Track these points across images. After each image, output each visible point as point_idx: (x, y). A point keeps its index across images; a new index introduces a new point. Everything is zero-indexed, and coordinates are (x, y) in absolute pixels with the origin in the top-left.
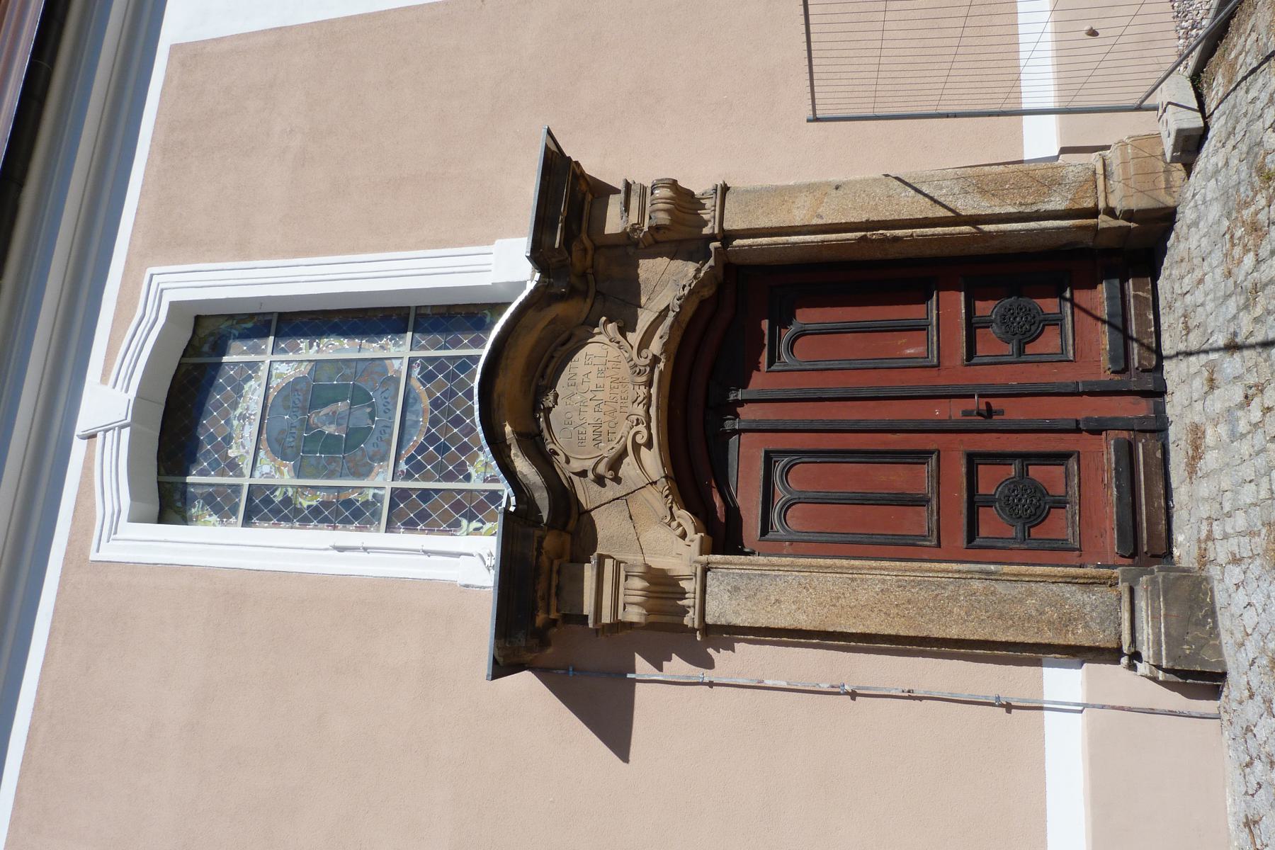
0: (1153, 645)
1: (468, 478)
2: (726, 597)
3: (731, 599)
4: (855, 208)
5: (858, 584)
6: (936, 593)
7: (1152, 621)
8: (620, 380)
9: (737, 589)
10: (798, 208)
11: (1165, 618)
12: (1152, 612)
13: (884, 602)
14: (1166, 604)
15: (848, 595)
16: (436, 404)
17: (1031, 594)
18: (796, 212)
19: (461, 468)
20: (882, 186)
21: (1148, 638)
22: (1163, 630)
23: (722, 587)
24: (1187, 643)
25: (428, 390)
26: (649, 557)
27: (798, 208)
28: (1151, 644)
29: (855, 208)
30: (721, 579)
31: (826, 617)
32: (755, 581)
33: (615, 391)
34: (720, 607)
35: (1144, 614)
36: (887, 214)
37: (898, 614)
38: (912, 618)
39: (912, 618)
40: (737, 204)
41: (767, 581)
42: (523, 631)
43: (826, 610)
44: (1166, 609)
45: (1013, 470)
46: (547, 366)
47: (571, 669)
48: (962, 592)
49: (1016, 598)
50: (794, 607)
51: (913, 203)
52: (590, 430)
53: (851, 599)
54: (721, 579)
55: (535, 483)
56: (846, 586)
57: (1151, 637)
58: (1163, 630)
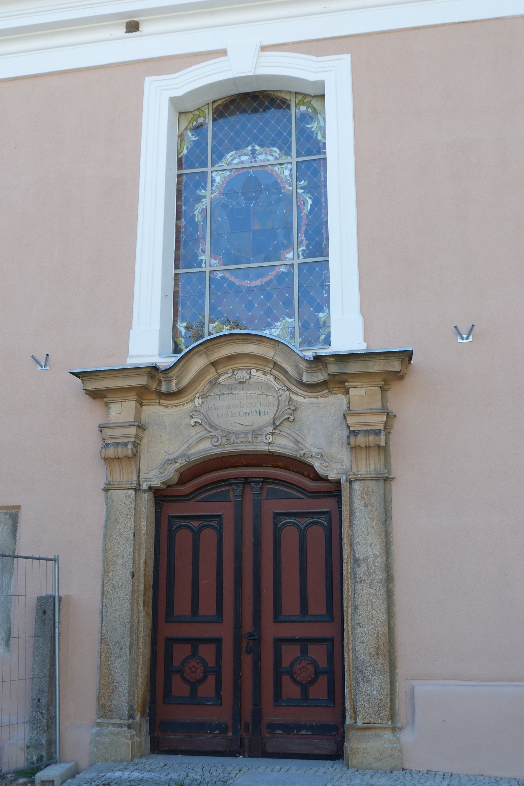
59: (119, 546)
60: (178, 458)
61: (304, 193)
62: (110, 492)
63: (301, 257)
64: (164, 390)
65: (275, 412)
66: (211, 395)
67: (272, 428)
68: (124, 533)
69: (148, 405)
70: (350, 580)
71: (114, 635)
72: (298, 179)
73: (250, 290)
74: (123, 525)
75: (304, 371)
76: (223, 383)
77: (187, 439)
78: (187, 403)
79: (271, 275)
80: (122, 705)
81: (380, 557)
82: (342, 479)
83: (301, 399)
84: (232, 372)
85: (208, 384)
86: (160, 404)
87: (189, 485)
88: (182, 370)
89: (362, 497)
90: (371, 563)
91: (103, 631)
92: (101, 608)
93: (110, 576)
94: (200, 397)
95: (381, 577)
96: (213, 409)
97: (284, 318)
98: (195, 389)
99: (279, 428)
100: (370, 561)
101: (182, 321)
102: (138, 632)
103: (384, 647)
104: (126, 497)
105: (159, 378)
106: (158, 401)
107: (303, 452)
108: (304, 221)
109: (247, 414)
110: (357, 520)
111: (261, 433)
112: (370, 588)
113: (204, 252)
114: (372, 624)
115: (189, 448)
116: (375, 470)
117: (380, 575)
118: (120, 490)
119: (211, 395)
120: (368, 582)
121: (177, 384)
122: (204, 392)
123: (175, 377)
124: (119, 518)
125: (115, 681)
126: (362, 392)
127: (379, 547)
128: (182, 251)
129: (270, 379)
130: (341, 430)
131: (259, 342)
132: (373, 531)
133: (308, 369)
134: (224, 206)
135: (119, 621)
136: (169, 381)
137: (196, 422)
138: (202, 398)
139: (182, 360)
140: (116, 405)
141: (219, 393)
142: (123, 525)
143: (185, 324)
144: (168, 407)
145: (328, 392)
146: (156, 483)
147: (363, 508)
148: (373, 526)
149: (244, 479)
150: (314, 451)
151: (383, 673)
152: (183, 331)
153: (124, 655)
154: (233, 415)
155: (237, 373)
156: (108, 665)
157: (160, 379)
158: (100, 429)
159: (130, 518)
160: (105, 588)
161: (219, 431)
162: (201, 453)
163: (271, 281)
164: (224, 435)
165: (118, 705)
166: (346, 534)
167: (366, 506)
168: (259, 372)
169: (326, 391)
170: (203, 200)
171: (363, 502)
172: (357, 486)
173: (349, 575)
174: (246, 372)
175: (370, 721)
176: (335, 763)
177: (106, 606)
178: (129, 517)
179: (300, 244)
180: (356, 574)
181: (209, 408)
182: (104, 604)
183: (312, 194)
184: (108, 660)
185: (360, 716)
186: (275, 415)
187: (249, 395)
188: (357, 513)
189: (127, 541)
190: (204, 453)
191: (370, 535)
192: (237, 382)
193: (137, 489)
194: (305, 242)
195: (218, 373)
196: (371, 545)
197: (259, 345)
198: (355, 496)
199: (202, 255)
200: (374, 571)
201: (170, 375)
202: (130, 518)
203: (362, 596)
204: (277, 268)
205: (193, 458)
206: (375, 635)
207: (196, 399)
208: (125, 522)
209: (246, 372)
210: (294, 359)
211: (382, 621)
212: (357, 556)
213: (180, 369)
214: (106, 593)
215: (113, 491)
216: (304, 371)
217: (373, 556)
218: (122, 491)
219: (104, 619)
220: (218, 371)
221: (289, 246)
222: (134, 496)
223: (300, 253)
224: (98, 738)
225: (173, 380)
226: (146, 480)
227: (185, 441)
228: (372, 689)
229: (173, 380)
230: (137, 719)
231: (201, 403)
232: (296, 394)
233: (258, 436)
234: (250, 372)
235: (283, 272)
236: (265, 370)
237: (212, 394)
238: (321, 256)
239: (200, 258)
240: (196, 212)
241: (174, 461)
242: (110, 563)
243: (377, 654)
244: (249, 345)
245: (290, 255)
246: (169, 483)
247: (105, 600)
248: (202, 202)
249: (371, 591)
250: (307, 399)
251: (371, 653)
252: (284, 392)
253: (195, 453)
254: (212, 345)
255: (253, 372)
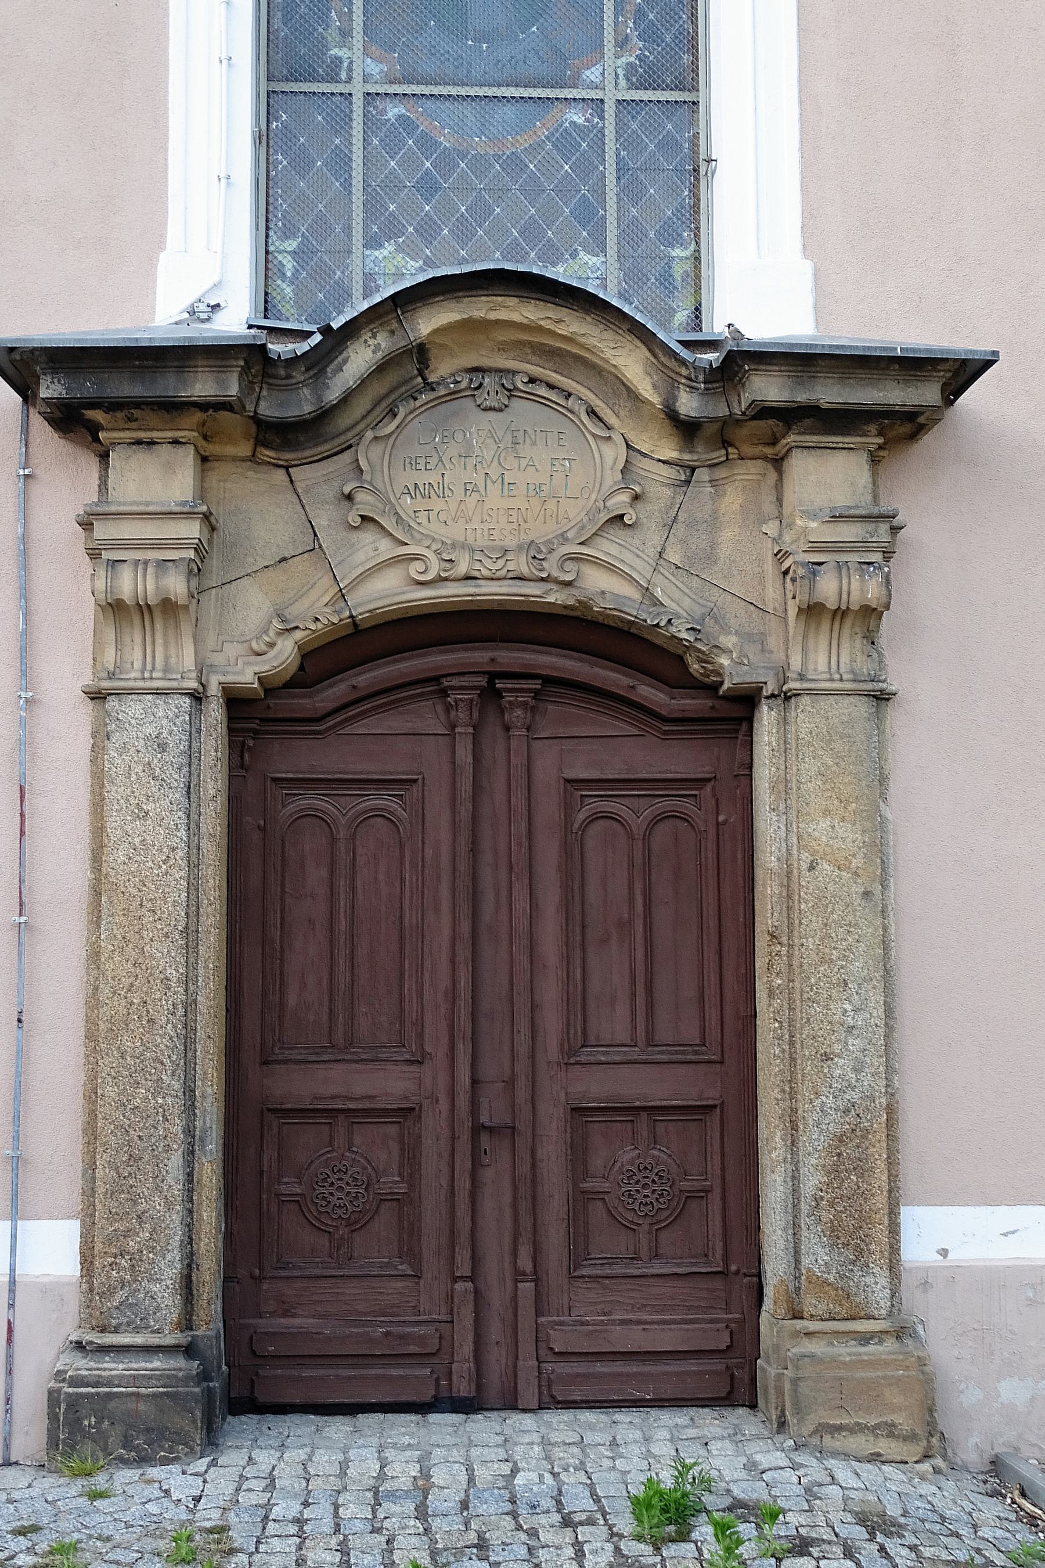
0: (95, 1376)
1: (372, 242)
2: (149, 730)
3: (147, 738)
4: (826, 925)
5: (177, 940)
6: (167, 1062)
7: (131, 1376)
8: (524, 526)
9: (163, 747)
10: (833, 827)
11: (132, 1394)
12: (144, 1376)
13: (149, 982)
14: (154, 1395)
15: (159, 927)
16: (514, 164)
17: (169, 1205)
18: (824, 824)
19: (392, 230)
20: (866, 971)
21: (105, 1370)
22: (116, 1390)
23: (165, 722)
24: (99, 1422)
25: (541, 145)
26: (217, 594)
27: (833, 827)
28: (97, 1372)
29: (826, 925)
30: (178, 722)
31: (123, 893)
32: (176, 776)
33: (503, 520)
34: (133, 722)
35: (143, 1365)
36: (813, 980)
37: (132, 1004)
38: (127, 1025)
39: (127, 1025)
40: (846, 719)
41: (177, 795)
42: (64, 392)
43: (135, 891)
44: (148, 1395)
45: (392, 1182)
46: (551, 387)
47: (27, 472)
48: (169, 1100)
49: (163, 1181)
50: (137, 841)
51: (830, 1023)
52: (433, 478)
53: (152, 932)
54: (178, 722)
55: (328, 387)
56: (173, 923)
57: (106, 1373)
58: (116, 1390)
62: (112, 703)
63: (623, 82)
87: (444, 657)
97: (574, 255)
113: (345, 34)
116: (852, 672)
152: (289, 265)
176: (822, 1437)
179: (622, 43)
193: (198, 697)
204: (556, 110)
223: (620, 71)
235: (573, 123)
238: (680, 87)
239: (335, 52)
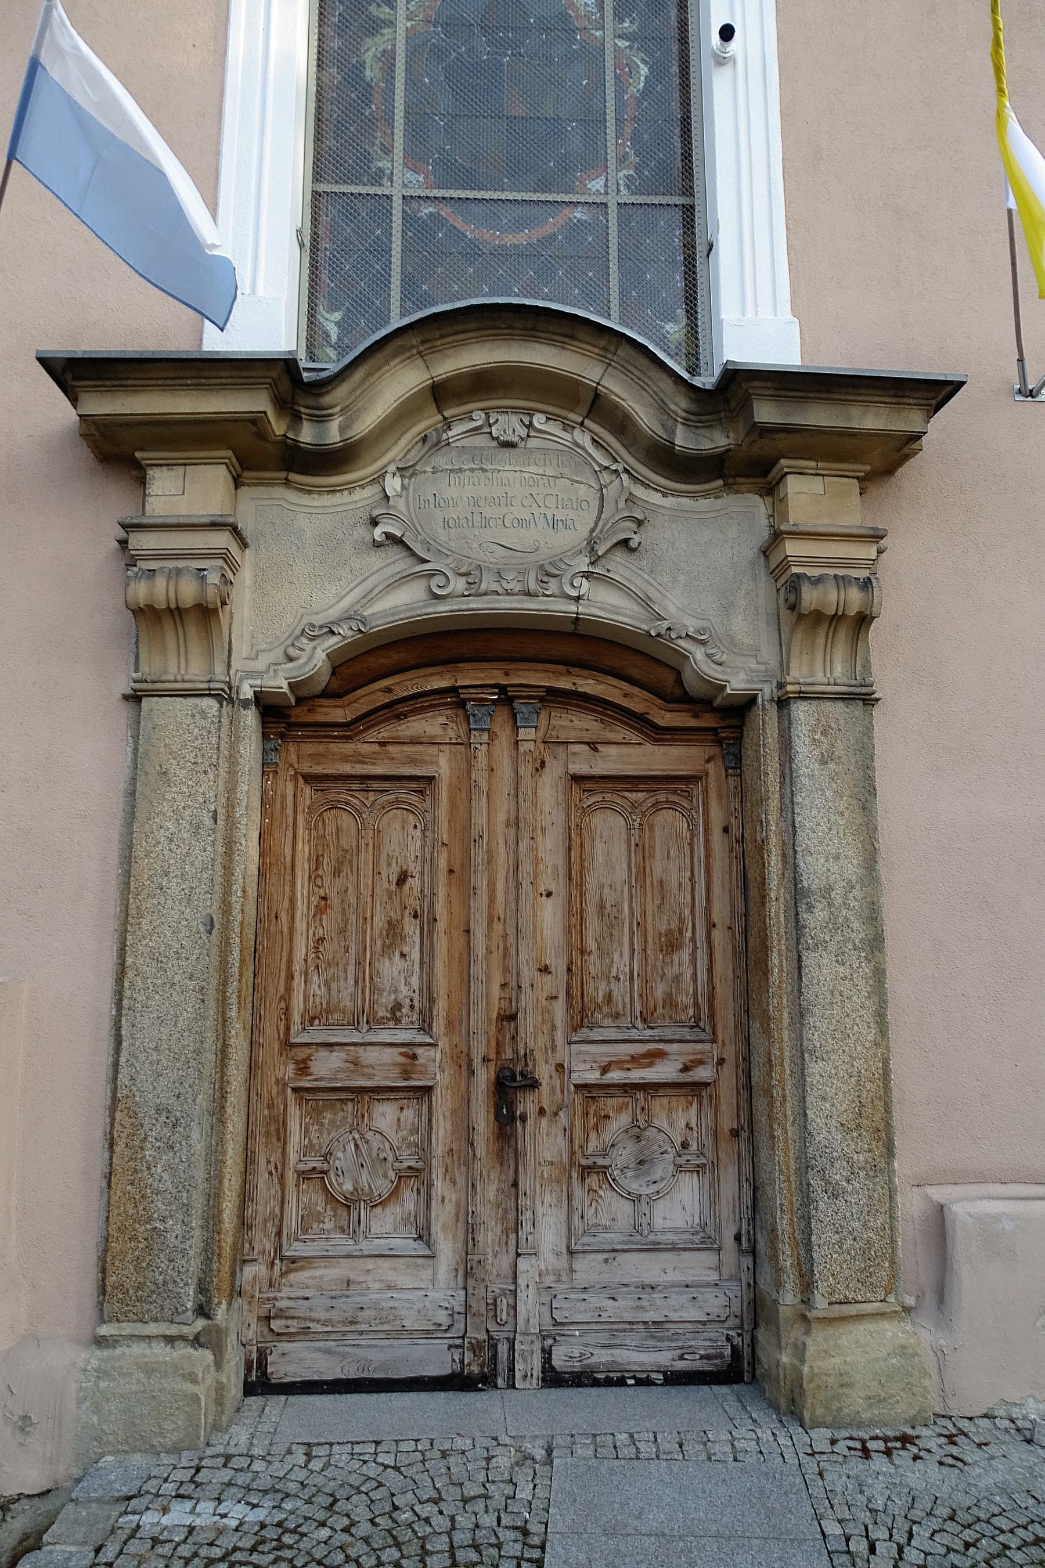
59: (173, 847)
60: (338, 622)
61: (630, 47)
64: (308, 440)
65: (592, 525)
66: (425, 472)
67: (587, 560)
68: (188, 812)
69: (255, 485)
70: (783, 942)
71: (155, 1088)
72: (618, 17)
73: (501, 254)
74: (185, 789)
75: (679, 420)
76: (459, 444)
77: (361, 578)
78: (362, 487)
79: (553, 224)
80: (175, 1281)
81: (858, 887)
82: (760, 696)
83: (655, 498)
84: (483, 415)
85: (417, 443)
86: (287, 483)
88: (358, 393)
89: (814, 740)
90: (839, 901)
91: (120, 1076)
92: (114, 1012)
93: (144, 927)
94: (398, 474)
95: (862, 935)
96: (432, 505)
98: (384, 454)
99: (603, 561)
100: (837, 896)
101: (332, 309)
102: (222, 1077)
103: (874, 1107)
104: (193, 716)
105: (297, 408)
106: (283, 474)
107: (666, 624)
108: (630, 112)
109: (520, 522)
110: (803, 795)
111: (558, 572)
112: (837, 961)
114: (844, 1051)
115: (368, 598)
117: (859, 932)
118: (177, 699)
119: (425, 472)
120: (833, 947)
121: (342, 429)
122: (409, 461)
123: (338, 409)
124: (173, 771)
125: (155, 1215)
126: (814, 486)
127: (855, 862)
128: (330, 142)
129: (581, 442)
130: (755, 578)
131: (566, 340)
132: (841, 822)
133: (691, 417)
134: (438, 53)
135: (169, 1049)
136: (321, 419)
137: (388, 536)
138: (401, 476)
139: (357, 367)
140: (171, 473)
141: (449, 467)
142: (185, 789)
143: (337, 316)
144: (310, 492)
145: (725, 485)
146: (279, 682)
147: (817, 766)
148: (840, 810)
149: (496, 690)
150: (691, 625)
151: (872, 1173)
152: (334, 332)
153: (184, 1143)
154: (486, 523)
155: (497, 420)
156: (136, 1171)
157: (300, 412)
158: (121, 534)
159: (205, 772)
160: (129, 960)
161: (449, 560)
162: (401, 612)
163: (552, 237)
164: (462, 570)
165: (165, 1282)
166: (773, 828)
167: (823, 762)
168: (551, 422)
169: (720, 482)
170: (385, 31)
171: (817, 752)
172: (801, 711)
173: (783, 930)
174: (521, 420)
175: (846, 1297)
177: (130, 1009)
178: (201, 768)
179: (622, 159)
180: (804, 927)
181: (422, 502)
182: (125, 1002)
183: (651, 55)
184: (136, 1159)
185: (822, 1287)
186: (592, 530)
187: (527, 475)
188: (802, 778)
189: (196, 833)
190: (409, 614)
191: (834, 832)
192: (494, 444)
194: (633, 158)
195: (445, 419)
196: (837, 858)
197: (563, 348)
198: (799, 737)
199: (381, 159)
200: (847, 919)
201: (327, 400)
202: (205, 772)
203: (819, 982)
204: (567, 211)
205: (380, 624)
206: (852, 1080)
207: (388, 477)
208: (190, 783)
209: (521, 420)
210: (655, 389)
211: (867, 1045)
212: (805, 884)
213: (353, 390)
214: (130, 974)
215: (157, 699)
216: (679, 420)
217: (843, 884)
218: (182, 699)
219: (125, 1044)
220: (447, 414)
221: (596, 163)
222: (216, 714)
224: (103, 1384)
225: (332, 415)
226: (249, 674)
227: (356, 582)
228: (847, 1215)
229: (332, 415)
230: (219, 1317)
231: (399, 489)
232: (642, 483)
233: (551, 579)
234: (531, 422)
236: (565, 421)
237: (429, 469)
240: (368, 57)
241: (326, 630)
242: (145, 891)
243: (859, 1126)
244: (537, 345)
245: (597, 185)
246: (305, 692)
247: (127, 993)
248: (382, 35)
249: (841, 969)
250: (670, 498)
251: (842, 1125)
252: (614, 477)
253: (384, 613)
254: (442, 337)
255: (538, 420)
